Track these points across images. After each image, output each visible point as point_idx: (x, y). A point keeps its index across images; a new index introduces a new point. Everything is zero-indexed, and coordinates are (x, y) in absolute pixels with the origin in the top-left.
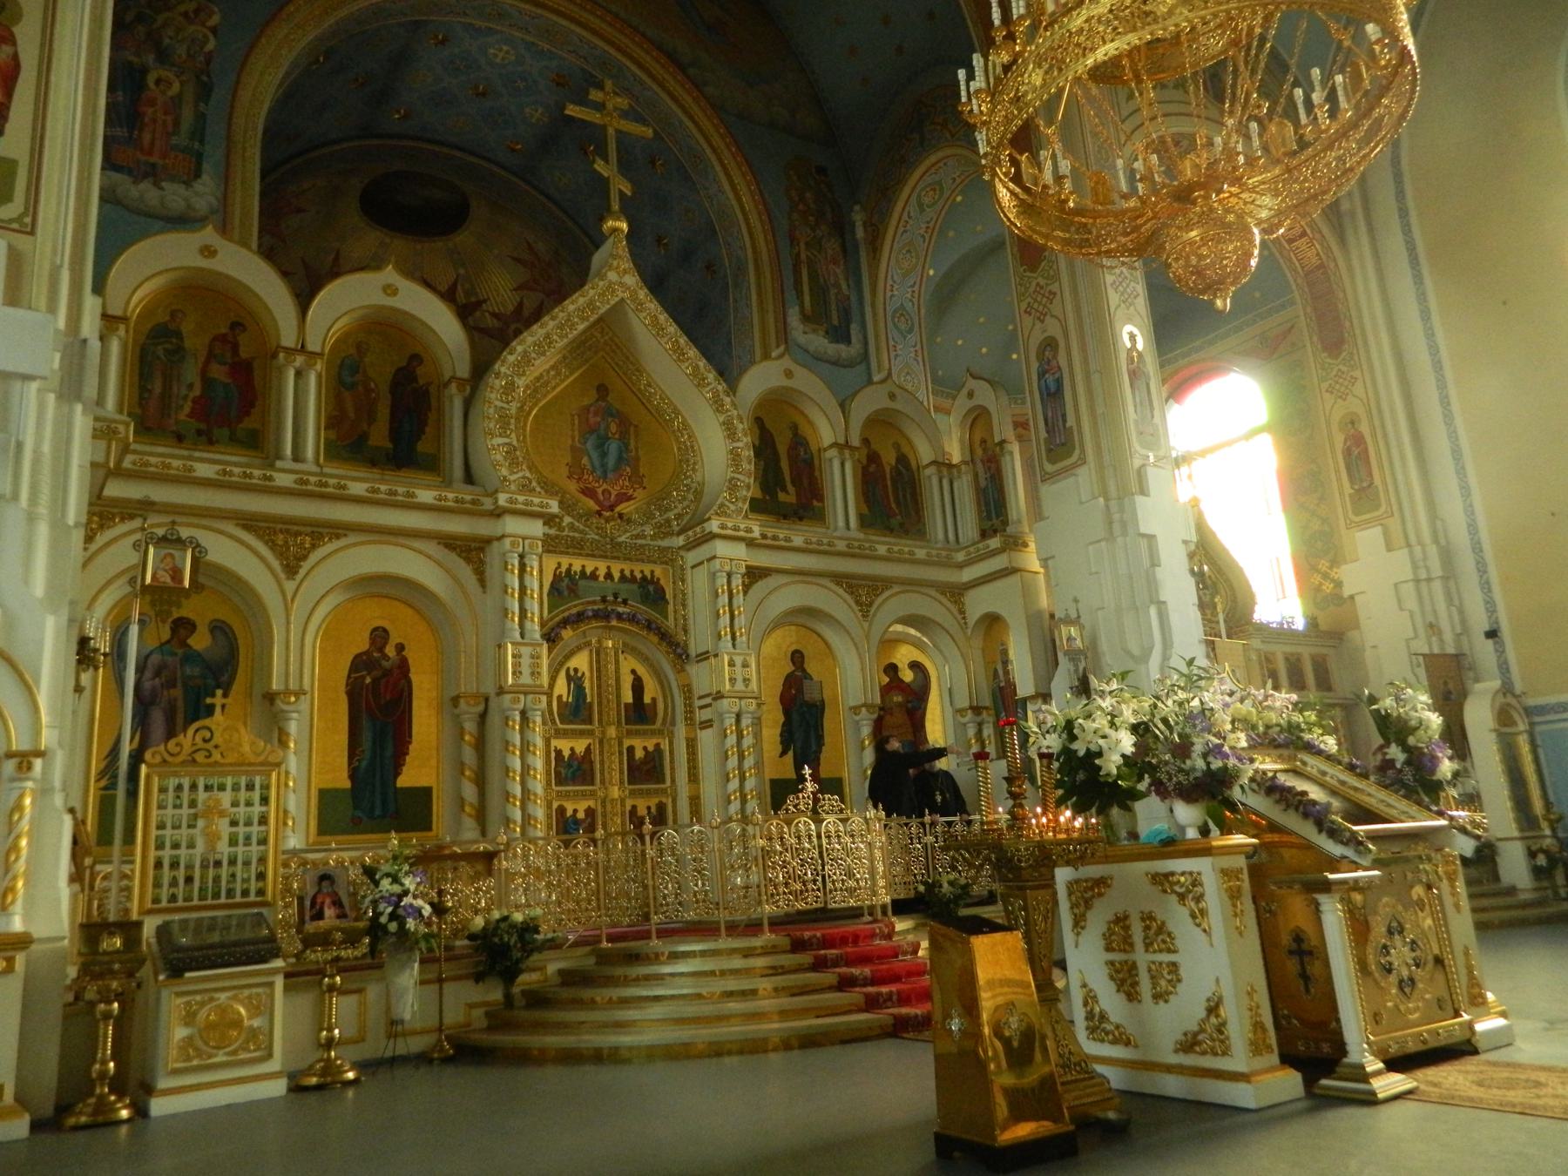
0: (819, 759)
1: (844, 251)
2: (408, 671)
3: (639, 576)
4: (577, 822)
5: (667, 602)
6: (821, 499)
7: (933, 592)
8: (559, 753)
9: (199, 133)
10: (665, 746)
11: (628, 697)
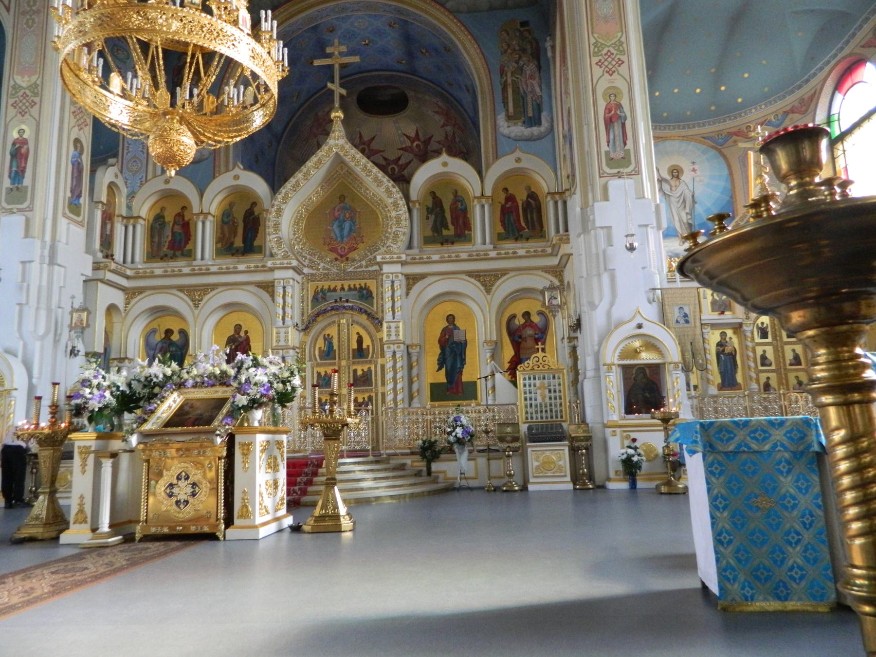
0: (462, 372)
1: (539, 68)
2: (249, 342)
3: (358, 286)
5: (373, 298)
6: (470, 230)
8: (319, 374)
10: (373, 368)
11: (354, 346)
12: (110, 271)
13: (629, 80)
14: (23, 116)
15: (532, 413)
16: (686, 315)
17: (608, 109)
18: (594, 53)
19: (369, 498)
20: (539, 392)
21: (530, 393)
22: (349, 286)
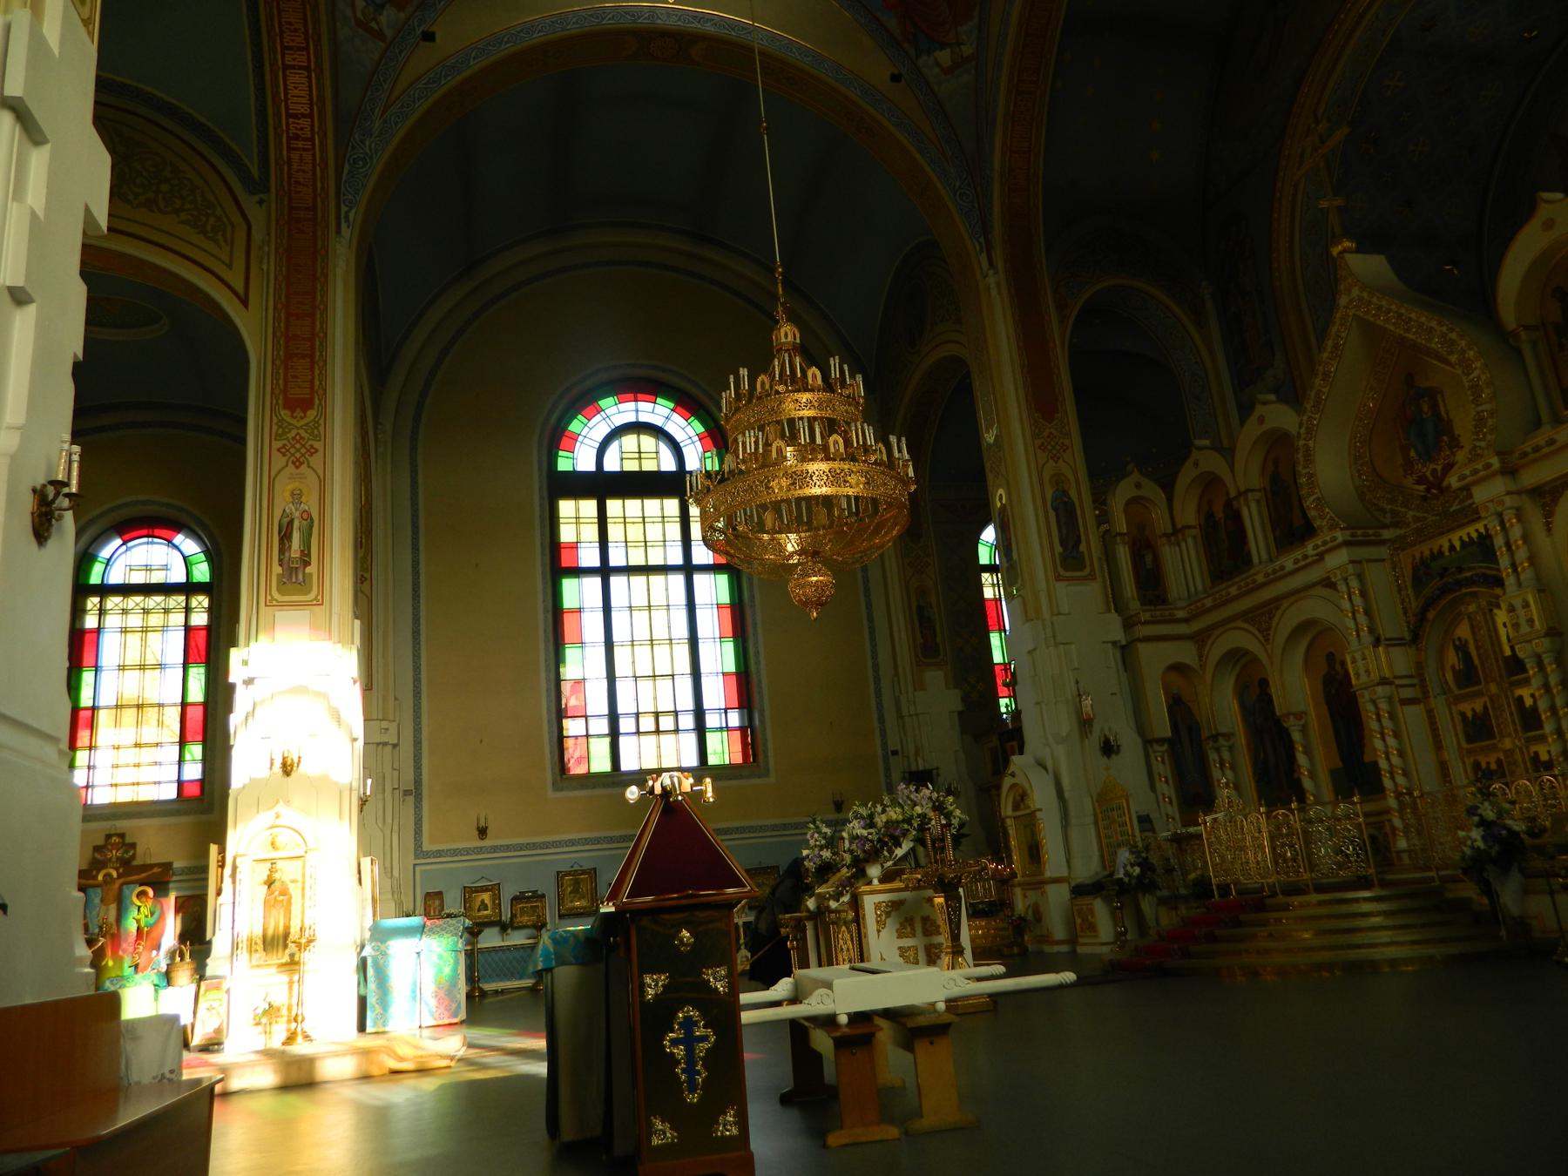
3: (1474, 535)
7: (1240, 623)
8: (1463, 715)
12: (1143, 624)
14: (297, 467)
18: (276, 435)
22: (1461, 538)
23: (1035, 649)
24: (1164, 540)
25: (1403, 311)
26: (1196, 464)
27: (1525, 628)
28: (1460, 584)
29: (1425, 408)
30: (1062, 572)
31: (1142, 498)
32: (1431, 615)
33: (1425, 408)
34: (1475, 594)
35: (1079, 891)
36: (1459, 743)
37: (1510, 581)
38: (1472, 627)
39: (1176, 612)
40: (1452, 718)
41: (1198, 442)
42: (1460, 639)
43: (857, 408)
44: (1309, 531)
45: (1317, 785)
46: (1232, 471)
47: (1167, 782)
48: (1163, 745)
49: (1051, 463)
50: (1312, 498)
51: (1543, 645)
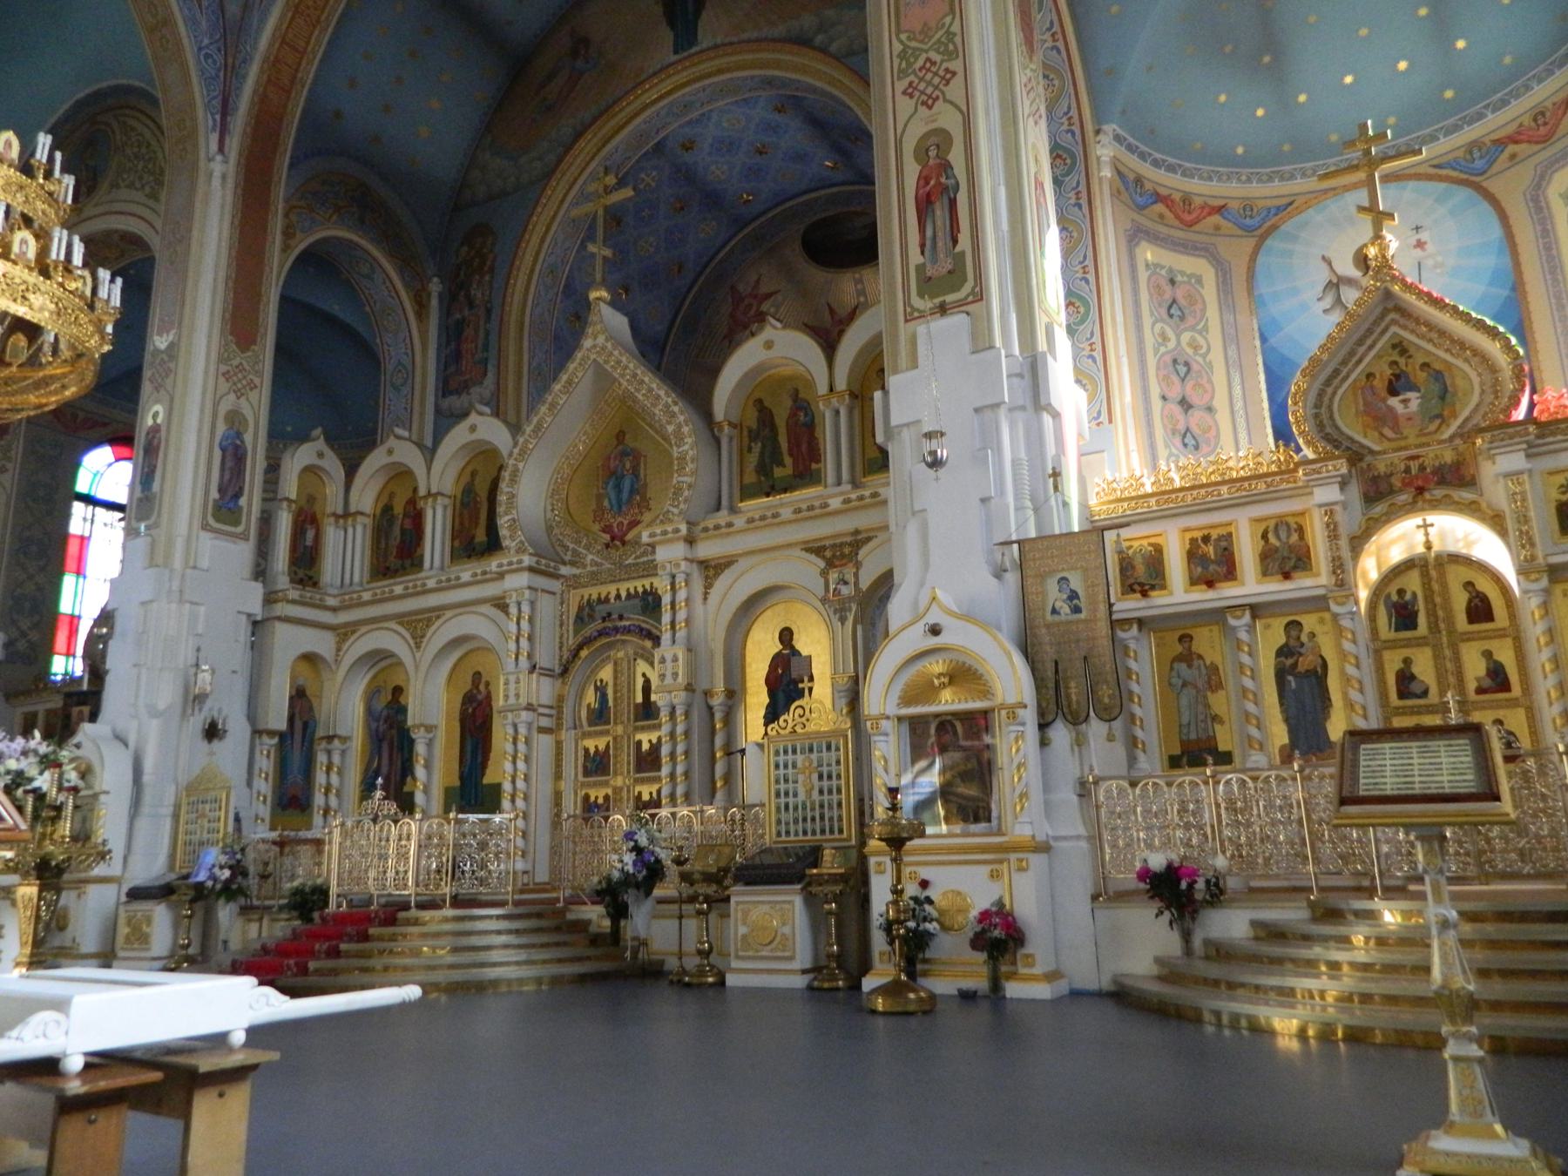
3: (640, 590)
4: (596, 805)
8: (587, 750)
9: (486, 347)
11: (639, 699)
12: (288, 601)
13: (964, 108)
14: (930, 108)
15: (787, 824)
16: (1073, 595)
17: (924, 179)
18: (900, 71)
19: (482, 982)
20: (801, 778)
21: (786, 781)
23: (151, 601)
24: (332, 520)
25: (639, 372)
26: (390, 452)
27: (669, 680)
28: (617, 630)
29: (628, 465)
30: (211, 521)
31: (319, 468)
32: (584, 653)
33: (628, 465)
34: (624, 642)
35: (136, 894)
36: (576, 775)
37: (666, 637)
38: (615, 671)
39: (327, 598)
40: (576, 752)
41: (399, 431)
42: (601, 681)
43: (57, 214)
44: (493, 545)
45: (428, 801)
46: (429, 469)
47: (266, 779)
48: (272, 738)
49: (232, 397)
50: (507, 518)
51: (679, 698)
